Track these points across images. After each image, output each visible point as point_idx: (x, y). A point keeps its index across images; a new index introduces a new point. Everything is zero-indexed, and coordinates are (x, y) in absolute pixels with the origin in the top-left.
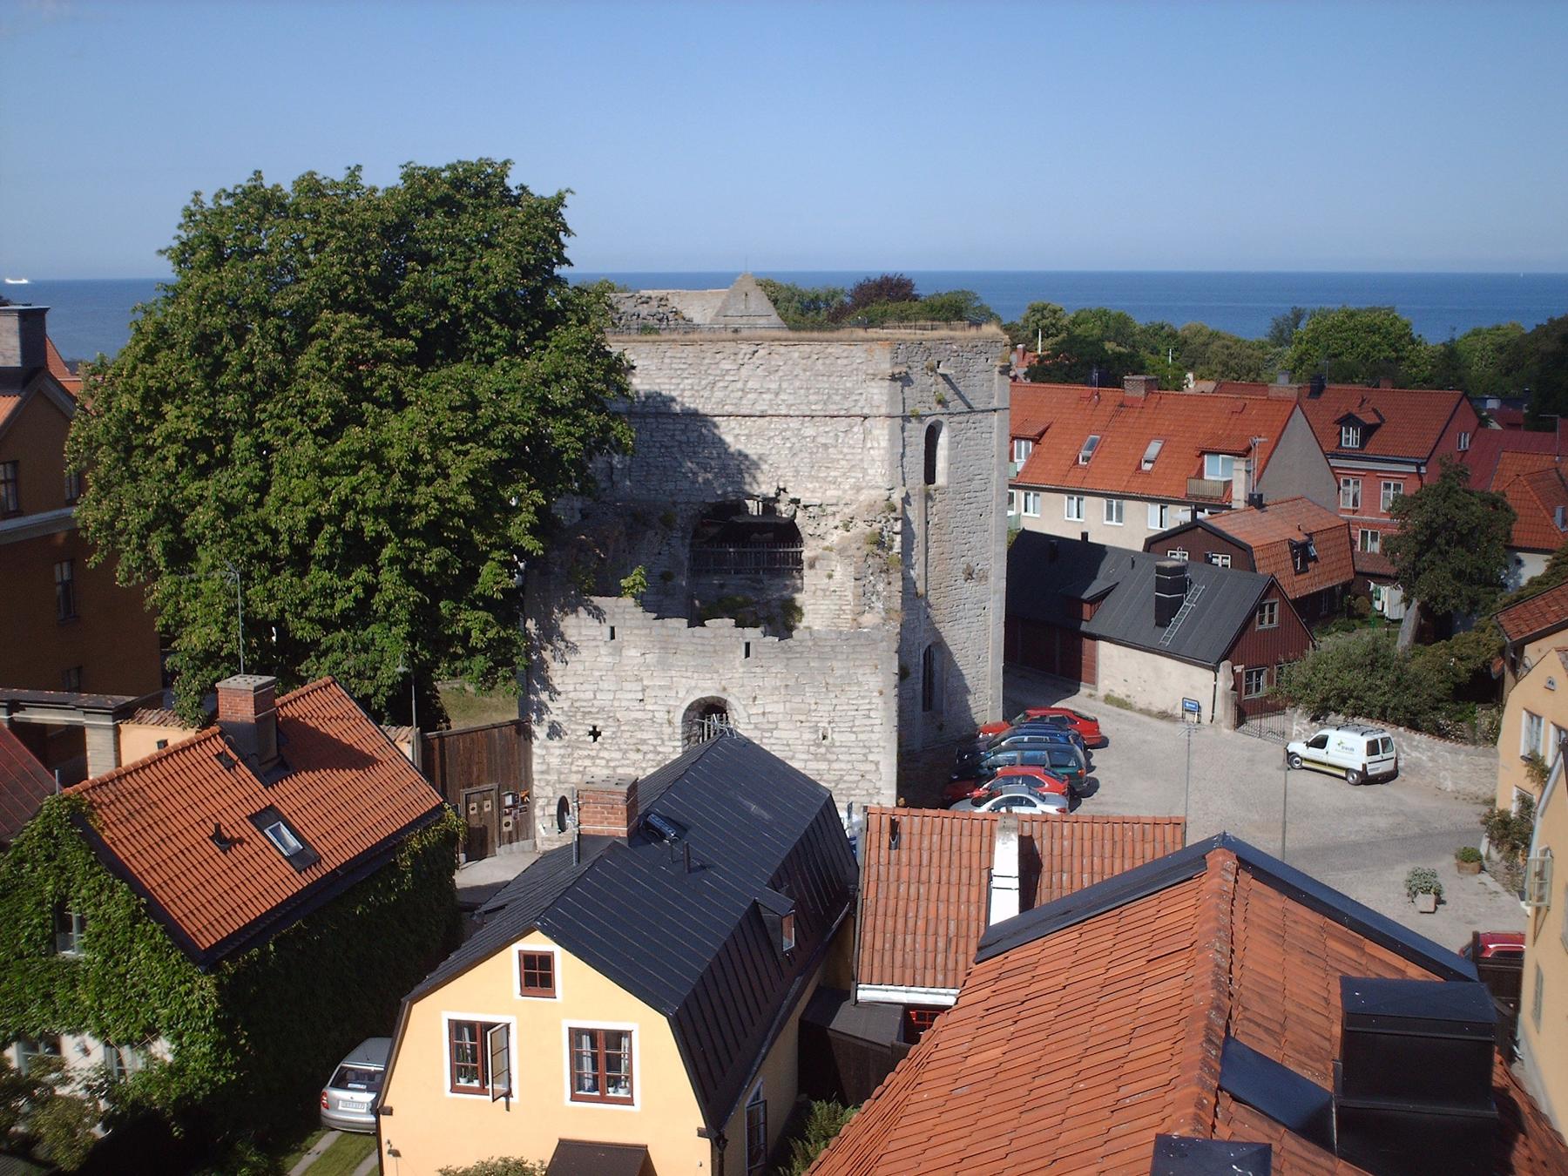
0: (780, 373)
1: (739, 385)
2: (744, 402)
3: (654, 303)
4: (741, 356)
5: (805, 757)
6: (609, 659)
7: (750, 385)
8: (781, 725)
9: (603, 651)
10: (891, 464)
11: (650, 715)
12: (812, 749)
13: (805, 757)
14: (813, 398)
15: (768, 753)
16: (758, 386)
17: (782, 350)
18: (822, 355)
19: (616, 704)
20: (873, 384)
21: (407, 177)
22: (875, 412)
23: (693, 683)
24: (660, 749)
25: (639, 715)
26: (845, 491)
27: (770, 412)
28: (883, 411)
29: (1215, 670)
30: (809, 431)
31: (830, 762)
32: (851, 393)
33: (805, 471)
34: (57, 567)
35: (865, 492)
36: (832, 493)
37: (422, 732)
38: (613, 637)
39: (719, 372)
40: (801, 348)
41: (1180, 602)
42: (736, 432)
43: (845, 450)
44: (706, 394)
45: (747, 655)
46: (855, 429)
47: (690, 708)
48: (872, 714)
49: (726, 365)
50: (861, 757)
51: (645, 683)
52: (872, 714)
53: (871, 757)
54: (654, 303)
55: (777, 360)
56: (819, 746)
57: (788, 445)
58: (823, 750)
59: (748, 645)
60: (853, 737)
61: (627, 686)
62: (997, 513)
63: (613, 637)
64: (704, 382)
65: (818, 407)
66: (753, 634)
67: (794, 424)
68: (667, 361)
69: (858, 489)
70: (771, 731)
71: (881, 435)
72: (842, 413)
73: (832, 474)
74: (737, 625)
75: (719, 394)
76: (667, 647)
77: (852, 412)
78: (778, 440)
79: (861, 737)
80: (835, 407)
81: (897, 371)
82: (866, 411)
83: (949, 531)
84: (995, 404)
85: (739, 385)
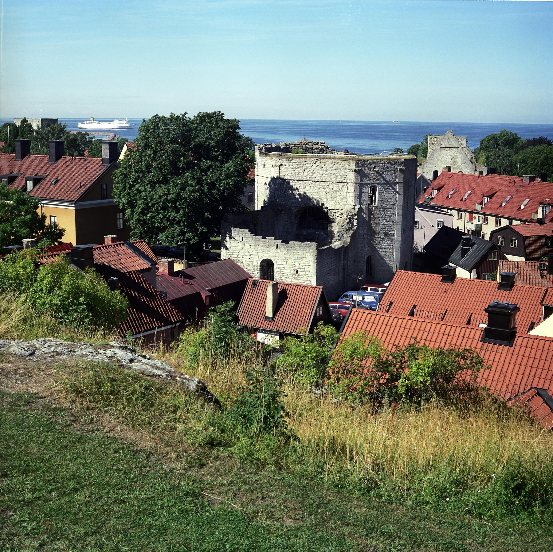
0: (323, 168)
1: (312, 171)
2: (313, 176)
3: (319, 145)
4: (312, 163)
5: (292, 278)
6: (242, 246)
7: (314, 172)
8: (285, 268)
9: (240, 244)
10: (355, 197)
11: (251, 263)
12: (294, 276)
13: (292, 278)
14: (332, 176)
15: (239, 267)
16: (317, 172)
17: (324, 161)
18: (336, 163)
19: (243, 259)
20: (350, 173)
21: (171, 116)
22: (350, 181)
23: (263, 255)
24: (254, 273)
25: (249, 263)
26: (341, 205)
27: (320, 180)
28: (353, 181)
29: (470, 272)
30: (331, 186)
31: (298, 280)
32: (344, 175)
33: (329, 198)
34: (118, 214)
35: (347, 206)
36: (337, 206)
37: (188, 262)
38: (243, 240)
39: (306, 167)
40: (330, 161)
41: (469, 250)
42: (310, 186)
43: (341, 193)
44: (302, 174)
45: (277, 248)
46: (345, 186)
47: (262, 261)
48: (310, 267)
49: (308, 165)
50: (306, 279)
51: (251, 254)
52: (310, 267)
53: (309, 279)
54: (319, 145)
55: (322, 164)
56: (295, 275)
57: (325, 190)
58: (296, 276)
59: (277, 244)
60: (304, 273)
61: (246, 254)
62: (398, 216)
63: (243, 240)
64: (301, 170)
65: (334, 179)
66: (279, 242)
67: (327, 184)
68: (291, 163)
69: (345, 205)
70: (283, 270)
71: (352, 187)
72: (341, 181)
73: (338, 200)
74: (263, 238)
75: (305, 174)
76: (256, 244)
77: (344, 181)
78: (322, 189)
79: (306, 273)
80: (339, 179)
81: (357, 169)
82: (348, 181)
83: (378, 220)
84: (398, 181)
85: (312, 171)
